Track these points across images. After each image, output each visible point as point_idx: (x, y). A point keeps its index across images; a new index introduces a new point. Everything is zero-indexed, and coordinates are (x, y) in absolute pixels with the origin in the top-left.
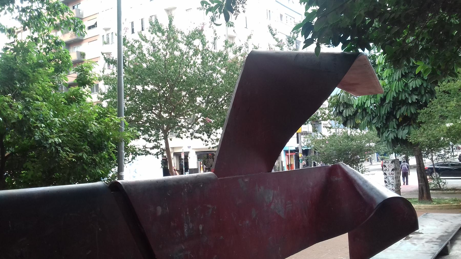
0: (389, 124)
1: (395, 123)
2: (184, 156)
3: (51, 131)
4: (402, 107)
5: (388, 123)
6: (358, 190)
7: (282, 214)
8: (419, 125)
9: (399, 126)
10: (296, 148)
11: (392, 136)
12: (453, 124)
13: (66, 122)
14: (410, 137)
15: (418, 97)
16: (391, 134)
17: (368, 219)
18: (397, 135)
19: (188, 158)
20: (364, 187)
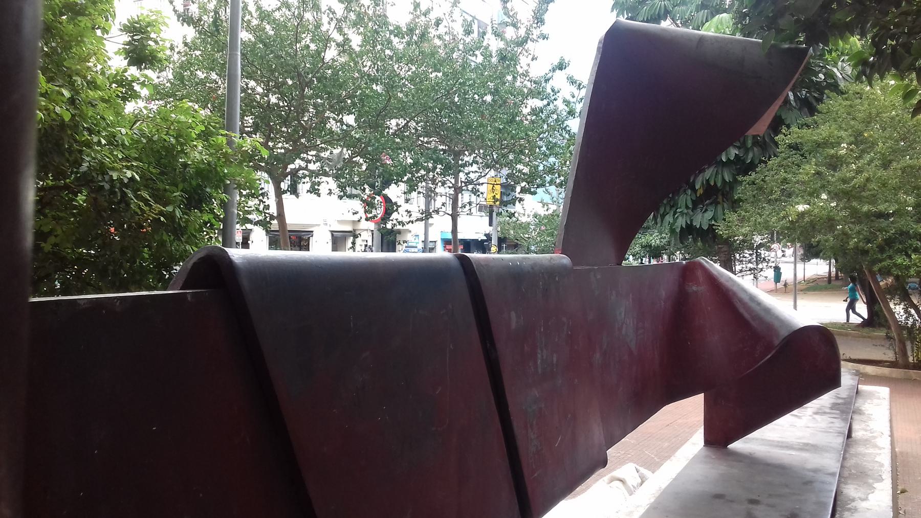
0: (678, 199)
1: (689, 198)
2: (241, 238)
3: (113, 155)
4: (708, 168)
5: (677, 198)
6: (742, 310)
7: (633, 345)
8: (735, 205)
9: (695, 204)
10: (485, 235)
11: (681, 222)
12: (808, 206)
13: (142, 138)
14: (719, 226)
15: (739, 152)
16: (680, 218)
17: (759, 364)
18: (691, 221)
19: (249, 242)
20: (753, 305)
